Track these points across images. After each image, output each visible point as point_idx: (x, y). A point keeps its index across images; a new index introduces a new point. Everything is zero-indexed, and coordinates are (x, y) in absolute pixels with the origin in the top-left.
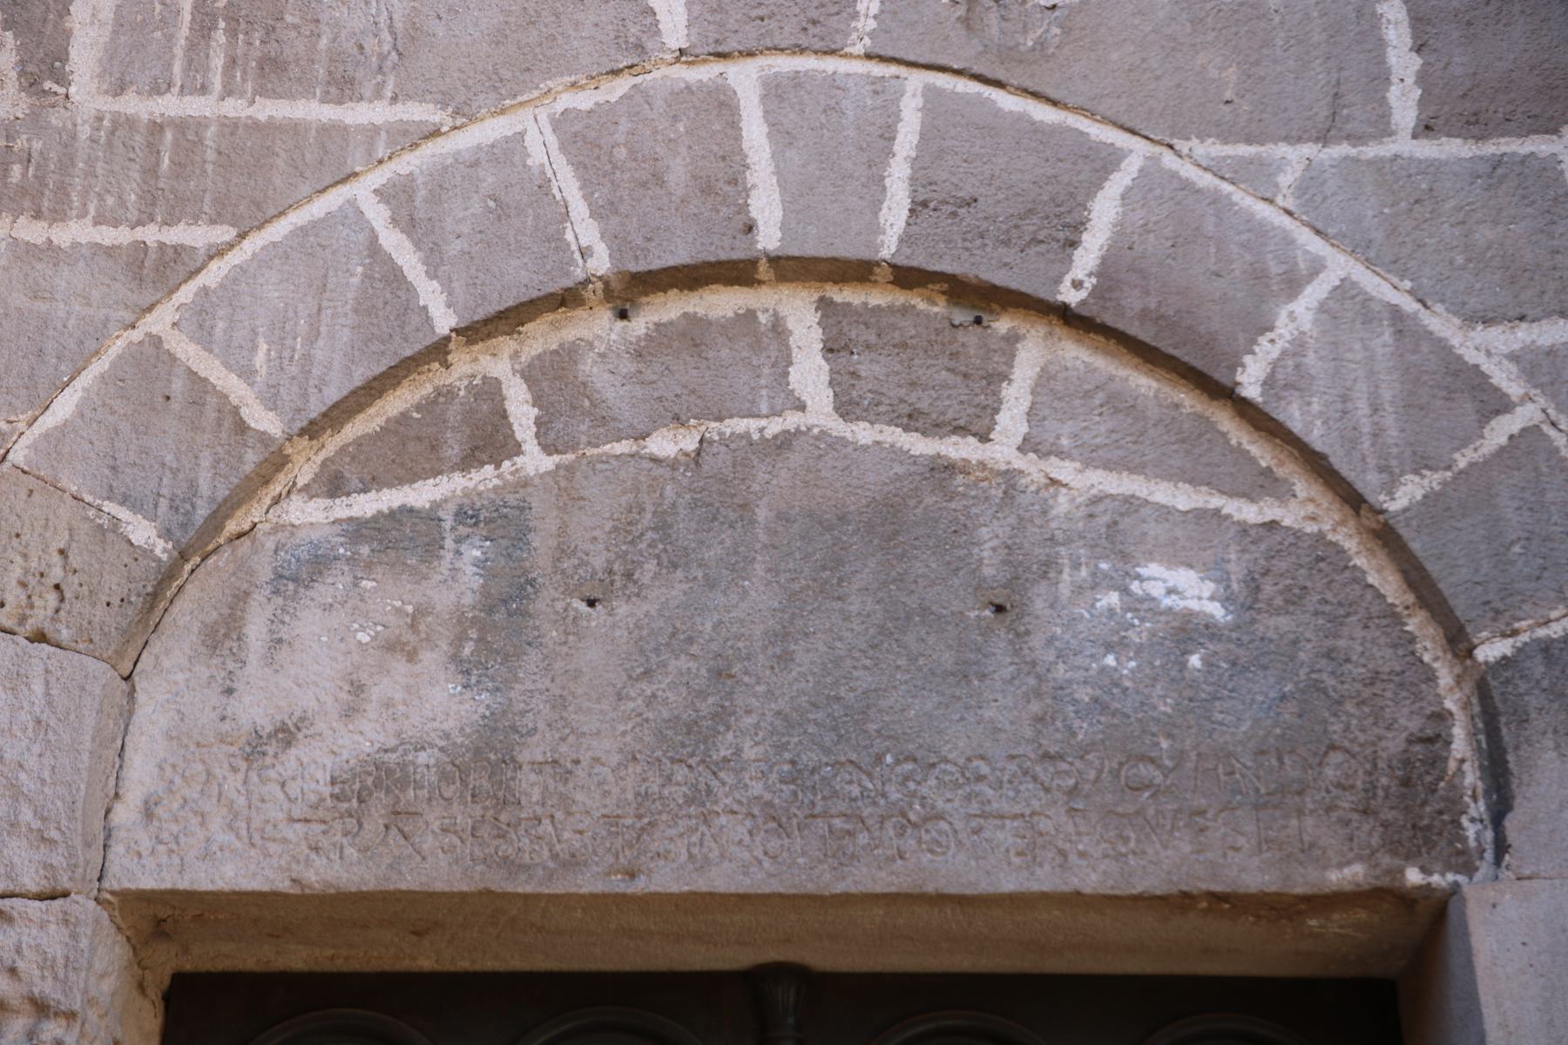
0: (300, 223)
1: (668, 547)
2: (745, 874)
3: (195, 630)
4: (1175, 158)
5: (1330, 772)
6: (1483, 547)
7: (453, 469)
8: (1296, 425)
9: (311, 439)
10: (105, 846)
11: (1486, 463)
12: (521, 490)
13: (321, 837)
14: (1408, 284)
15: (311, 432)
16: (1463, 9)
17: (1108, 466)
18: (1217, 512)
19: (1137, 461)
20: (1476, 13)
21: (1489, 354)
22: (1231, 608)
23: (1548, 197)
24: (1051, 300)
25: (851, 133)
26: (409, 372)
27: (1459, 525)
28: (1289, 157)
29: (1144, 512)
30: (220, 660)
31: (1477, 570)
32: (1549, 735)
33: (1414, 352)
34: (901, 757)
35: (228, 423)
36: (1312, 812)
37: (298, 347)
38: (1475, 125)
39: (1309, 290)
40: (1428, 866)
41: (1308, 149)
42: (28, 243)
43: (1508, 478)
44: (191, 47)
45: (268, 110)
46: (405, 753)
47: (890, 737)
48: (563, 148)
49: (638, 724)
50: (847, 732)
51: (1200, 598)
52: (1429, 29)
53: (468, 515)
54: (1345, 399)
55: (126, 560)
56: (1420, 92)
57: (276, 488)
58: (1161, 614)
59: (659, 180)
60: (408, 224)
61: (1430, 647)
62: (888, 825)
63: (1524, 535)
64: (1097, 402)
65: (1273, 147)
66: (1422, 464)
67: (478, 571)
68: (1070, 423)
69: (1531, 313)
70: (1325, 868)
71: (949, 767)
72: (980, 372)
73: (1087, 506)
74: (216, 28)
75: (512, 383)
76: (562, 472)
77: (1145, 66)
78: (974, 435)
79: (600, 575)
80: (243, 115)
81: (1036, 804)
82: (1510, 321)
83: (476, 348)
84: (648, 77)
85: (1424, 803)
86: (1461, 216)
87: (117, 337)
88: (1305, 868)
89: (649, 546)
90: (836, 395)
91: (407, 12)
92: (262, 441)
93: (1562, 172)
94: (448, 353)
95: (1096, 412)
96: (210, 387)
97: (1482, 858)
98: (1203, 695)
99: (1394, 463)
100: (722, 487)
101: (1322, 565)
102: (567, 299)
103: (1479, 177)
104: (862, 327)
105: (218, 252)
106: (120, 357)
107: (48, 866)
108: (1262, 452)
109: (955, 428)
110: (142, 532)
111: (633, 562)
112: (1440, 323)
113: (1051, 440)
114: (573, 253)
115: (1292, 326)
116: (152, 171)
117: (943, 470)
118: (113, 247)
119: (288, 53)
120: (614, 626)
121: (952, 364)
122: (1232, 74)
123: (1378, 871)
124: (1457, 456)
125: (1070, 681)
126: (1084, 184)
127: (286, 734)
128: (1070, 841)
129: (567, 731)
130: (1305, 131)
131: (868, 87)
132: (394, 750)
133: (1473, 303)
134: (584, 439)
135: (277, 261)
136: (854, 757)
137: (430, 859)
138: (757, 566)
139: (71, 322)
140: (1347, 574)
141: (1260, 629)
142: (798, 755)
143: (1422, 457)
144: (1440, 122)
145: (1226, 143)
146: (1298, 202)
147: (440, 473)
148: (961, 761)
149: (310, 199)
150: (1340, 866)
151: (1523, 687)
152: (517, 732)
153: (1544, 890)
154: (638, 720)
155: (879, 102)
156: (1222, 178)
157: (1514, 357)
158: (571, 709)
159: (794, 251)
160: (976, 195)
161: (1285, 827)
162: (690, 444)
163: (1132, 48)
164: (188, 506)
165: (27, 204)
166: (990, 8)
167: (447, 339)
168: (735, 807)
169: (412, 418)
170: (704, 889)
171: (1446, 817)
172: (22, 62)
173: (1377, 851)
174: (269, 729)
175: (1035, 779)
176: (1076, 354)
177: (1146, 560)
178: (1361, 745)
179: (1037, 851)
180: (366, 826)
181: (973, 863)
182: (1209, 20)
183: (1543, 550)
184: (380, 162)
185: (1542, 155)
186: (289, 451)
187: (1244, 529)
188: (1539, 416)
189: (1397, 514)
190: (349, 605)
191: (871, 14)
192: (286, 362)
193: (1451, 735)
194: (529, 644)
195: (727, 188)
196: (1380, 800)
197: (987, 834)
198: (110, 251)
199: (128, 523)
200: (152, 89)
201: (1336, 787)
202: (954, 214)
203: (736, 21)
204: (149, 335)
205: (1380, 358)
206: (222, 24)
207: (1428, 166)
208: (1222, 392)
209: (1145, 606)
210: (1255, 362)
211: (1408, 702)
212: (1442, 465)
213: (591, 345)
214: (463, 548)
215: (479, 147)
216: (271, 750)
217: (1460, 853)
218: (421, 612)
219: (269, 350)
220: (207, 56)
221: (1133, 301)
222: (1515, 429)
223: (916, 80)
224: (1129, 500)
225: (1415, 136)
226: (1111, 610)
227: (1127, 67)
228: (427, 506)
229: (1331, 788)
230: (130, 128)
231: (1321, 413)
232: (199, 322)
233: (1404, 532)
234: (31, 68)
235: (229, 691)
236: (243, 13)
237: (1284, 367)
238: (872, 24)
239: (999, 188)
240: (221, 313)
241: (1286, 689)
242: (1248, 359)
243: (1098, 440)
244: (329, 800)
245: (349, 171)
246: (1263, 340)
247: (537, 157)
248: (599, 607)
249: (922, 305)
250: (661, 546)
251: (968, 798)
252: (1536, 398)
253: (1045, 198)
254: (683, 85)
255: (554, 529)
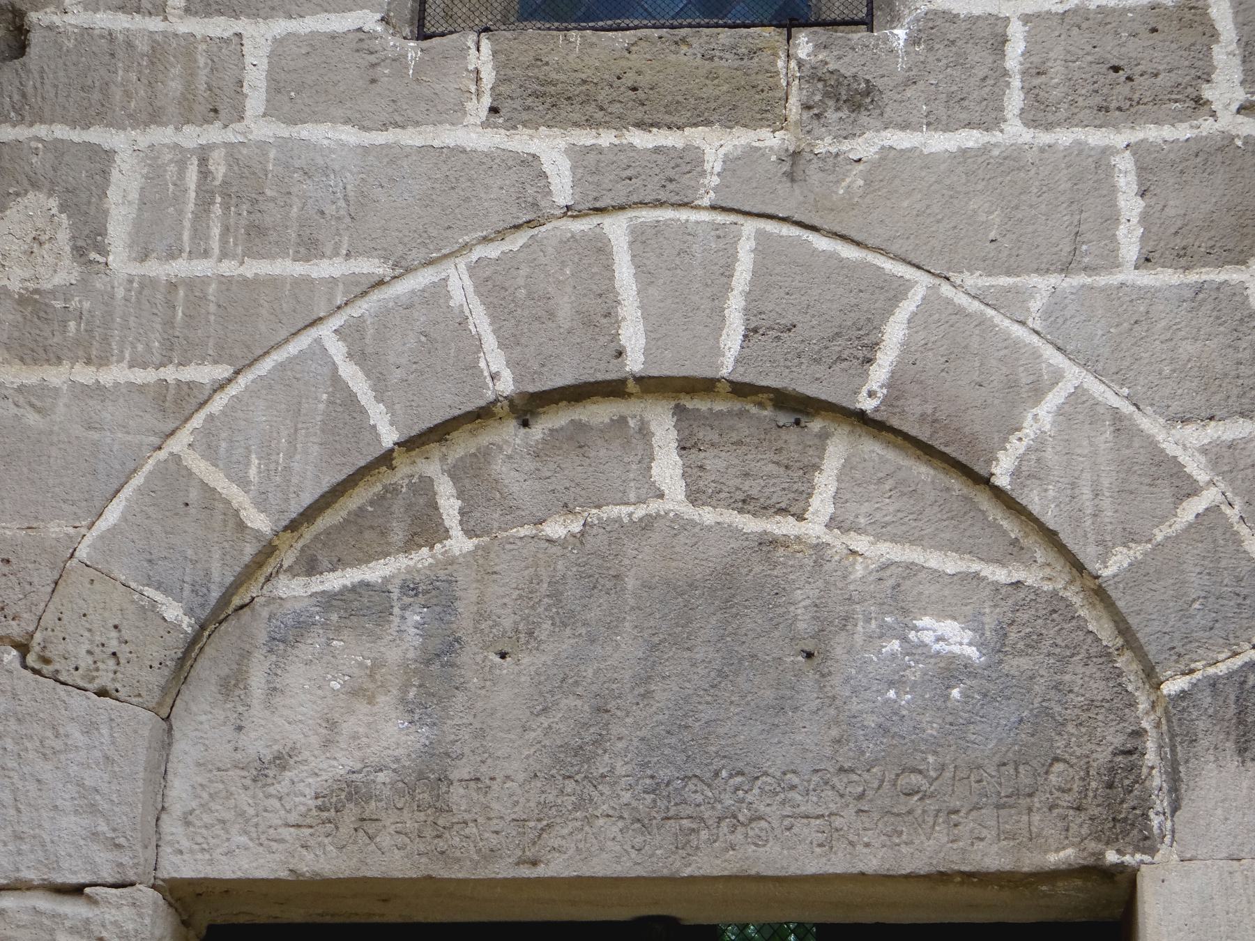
0: (280, 360)
1: (560, 610)
2: (618, 863)
3: (214, 681)
4: (950, 288)
5: (1053, 778)
6: (1171, 604)
7: (398, 552)
8: (1035, 509)
9: (292, 532)
10: (157, 846)
11: (1177, 536)
12: (449, 567)
13: (309, 838)
14: (1125, 391)
15: (293, 526)
16: (1178, 160)
17: (894, 539)
18: (976, 576)
19: (916, 535)
20: (1187, 163)
21: (1185, 448)
22: (984, 651)
23: (1236, 318)
24: (852, 407)
25: (700, 272)
26: (363, 476)
27: (1154, 587)
28: (1039, 286)
29: (922, 575)
30: (233, 704)
31: (1166, 623)
32: (1211, 751)
33: (1128, 447)
34: (734, 772)
35: (231, 524)
36: (1039, 809)
37: (281, 460)
38: (1184, 258)
39: (1050, 395)
40: (1122, 849)
41: (1054, 279)
42: (83, 384)
43: (1194, 548)
44: (197, 217)
45: (255, 268)
46: (368, 773)
47: (725, 757)
48: (477, 292)
49: (538, 750)
50: (693, 753)
51: (961, 644)
52: (1151, 177)
53: (410, 588)
54: (1073, 485)
55: (162, 633)
56: (1142, 230)
57: (268, 569)
58: (931, 657)
59: (552, 315)
60: (358, 356)
61: (1133, 682)
62: (724, 824)
63: (1203, 594)
64: (888, 487)
65: (1027, 278)
66: (1130, 538)
67: (418, 632)
68: (866, 504)
69: (1218, 414)
70: (1046, 852)
71: (769, 779)
72: (798, 464)
73: (877, 571)
74: (214, 203)
75: (441, 481)
76: (480, 552)
77: (928, 211)
78: (793, 515)
79: (509, 634)
80: (235, 273)
81: (833, 807)
82: (1202, 421)
83: (413, 453)
84: (543, 229)
85: (1122, 802)
86: (1168, 335)
87: (149, 457)
88: (1032, 852)
89: (546, 609)
90: (687, 485)
91: (357, 183)
92: (256, 538)
93: (1247, 296)
94: (393, 459)
95: (887, 495)
96: (217, 496)
97: (1163, 842)
98: (961, 721)
99: (1108, 538)
100: (600, 562)
101: (1055, 616)
102: (482, 415)
103: (1184, 301)
104: (709, 428)
105: (221, 386)
106: (150, 472)
107: (121, 865)
108: (1011, 527)
109: (779, 510)
110: (173, 611)
111: (534, 623)
112: (1149, 424)
113: (851, 518)
114: (485, 378)
115: (1035, 426)
116: (169, 323)
117: (769, 543)
118: (144, 385)
119: (268, 220)
120: (519, 673)
121: (776, 458)
122: (996, 217)
123: (1085, 854)
124: (1156, 531)
125: (861, 712)
126: (880, 311)
127: (281, 761)
128: (858, 835)
129: (486, 755)
130: (1052, 264)
131: (713, 233)
132: (360, 772)
133: (1176, 407)
134: (496, 525)
135: (264, 392)
136: (698, 772)
137: (387, 854)
138: (627, 624)
139: (115, 448)
140: (1074, 623)
141: (1005, 668)
142: (657, 772)
143: (1130, 533)
144: (1157, 255)
145: (990, 276)
146: (1044, 323)
147: (388, 554)
148: (778, 774)
149: (287, 341)
150: (1057, 850)
151: (1195, 714)
152: (449, 756)
153: (1199, 869)
154: (538, 746)
155: (721, 246)
156: (987, 304)
157: (1204, 451)
158: (488, 738)
159: (655, 372)
160: (795, 322)
161: (1018, 822)
162: (576, 527)
163: (919, 196)
164: (204, 590)
165: (81, 353)
166: (810, 160)
167: (392, 451)
168: (611, 812)
169: (367, 510)
170: (588, 874)
171: (1138, 812)
172: (74, 238)
173: (1086, 838)
174: (270, 757)
175: (833, 788)
176: (873, 449)
177: (921, 614)
178: (1078, 758)
179: (834, 842)
180: (341, 830)
181: (785, 852)
182: (980, 171)
183: (1217, 606)
184: (339, 308)
185: (1233, 283)
186: (276, 542)
187: (997, 587)
188: (1220, 498)
189: (1109, 578)
190: (324, 660)
191: (715, 172)
192: (272, 473)
193: (1145, 748)
194: (457, 688)
195: (604, 321)
196: (1090, 800)
197: (795, 830)
198: (142, 389)
199: (163, 604)
200: (168, 255)
201: (1058, 790)
202: (778, 338)
203: (610, 181)
204: (171, 454)
205: (1102, 452)
206: (218, 199)
207: (1146, 293)
208: (983, 481)
209: (919, 651)
210: (1007, 456)
211: (1114, 723)
212: (1144, 539)
213: (500, 449)
214: (407, 614)
215: (413, 292)
216: (271, 773)
217: (1146, 838)
218: (377, 665)
219: (260, 464)
220: (208, 227)
221: (914, 407)
222: (1201, 509)
223: (750, 227)
224: (910, 566)
225: (1136, 268)
226: (893, 655)
227: (915, 213)
228: (380, 581)
229: (1053, 790)
230: (153, 288)
231: (1055, 498)
232: (207, 444)
233: (1113, 594)
234: (80, 243)
235: (240, 728)
236: (234, 189)
237: (1029, 461)
238: (716, 180)
239: (813, 316)
240: (224, 435)
241: (1024, 715)
242: (1001, 454)
243: (887, 519)
244: (314, 810)
245: (315, 317)
246: (1013, 439)
247: (457, 298)
248: (508, 659)
249: (754, 410)
250: (554, 610)
251: (783, 803)
252: (1218, 484)
253: (849, 323)
254: (569, 235)
255: (474, 599)
